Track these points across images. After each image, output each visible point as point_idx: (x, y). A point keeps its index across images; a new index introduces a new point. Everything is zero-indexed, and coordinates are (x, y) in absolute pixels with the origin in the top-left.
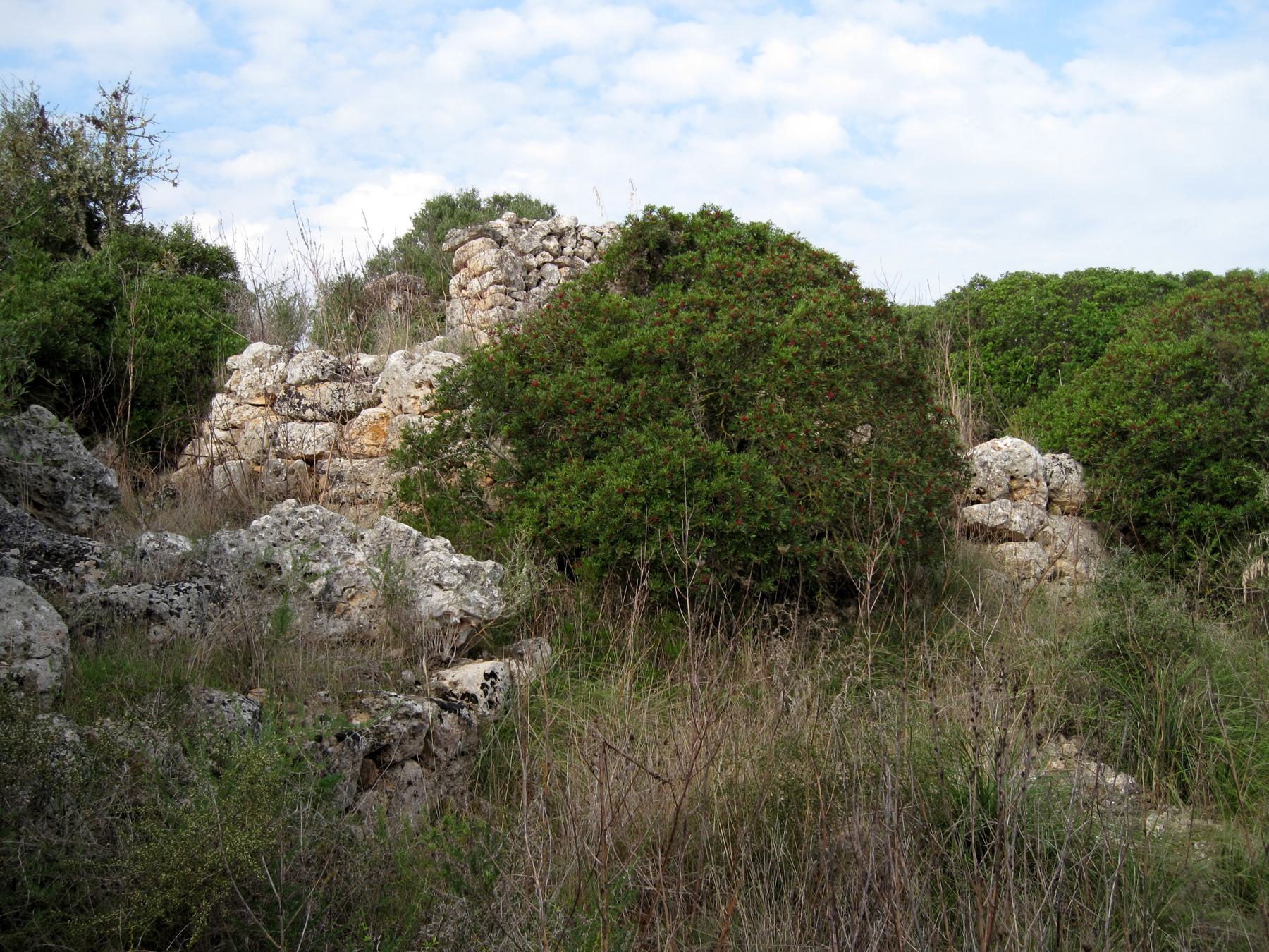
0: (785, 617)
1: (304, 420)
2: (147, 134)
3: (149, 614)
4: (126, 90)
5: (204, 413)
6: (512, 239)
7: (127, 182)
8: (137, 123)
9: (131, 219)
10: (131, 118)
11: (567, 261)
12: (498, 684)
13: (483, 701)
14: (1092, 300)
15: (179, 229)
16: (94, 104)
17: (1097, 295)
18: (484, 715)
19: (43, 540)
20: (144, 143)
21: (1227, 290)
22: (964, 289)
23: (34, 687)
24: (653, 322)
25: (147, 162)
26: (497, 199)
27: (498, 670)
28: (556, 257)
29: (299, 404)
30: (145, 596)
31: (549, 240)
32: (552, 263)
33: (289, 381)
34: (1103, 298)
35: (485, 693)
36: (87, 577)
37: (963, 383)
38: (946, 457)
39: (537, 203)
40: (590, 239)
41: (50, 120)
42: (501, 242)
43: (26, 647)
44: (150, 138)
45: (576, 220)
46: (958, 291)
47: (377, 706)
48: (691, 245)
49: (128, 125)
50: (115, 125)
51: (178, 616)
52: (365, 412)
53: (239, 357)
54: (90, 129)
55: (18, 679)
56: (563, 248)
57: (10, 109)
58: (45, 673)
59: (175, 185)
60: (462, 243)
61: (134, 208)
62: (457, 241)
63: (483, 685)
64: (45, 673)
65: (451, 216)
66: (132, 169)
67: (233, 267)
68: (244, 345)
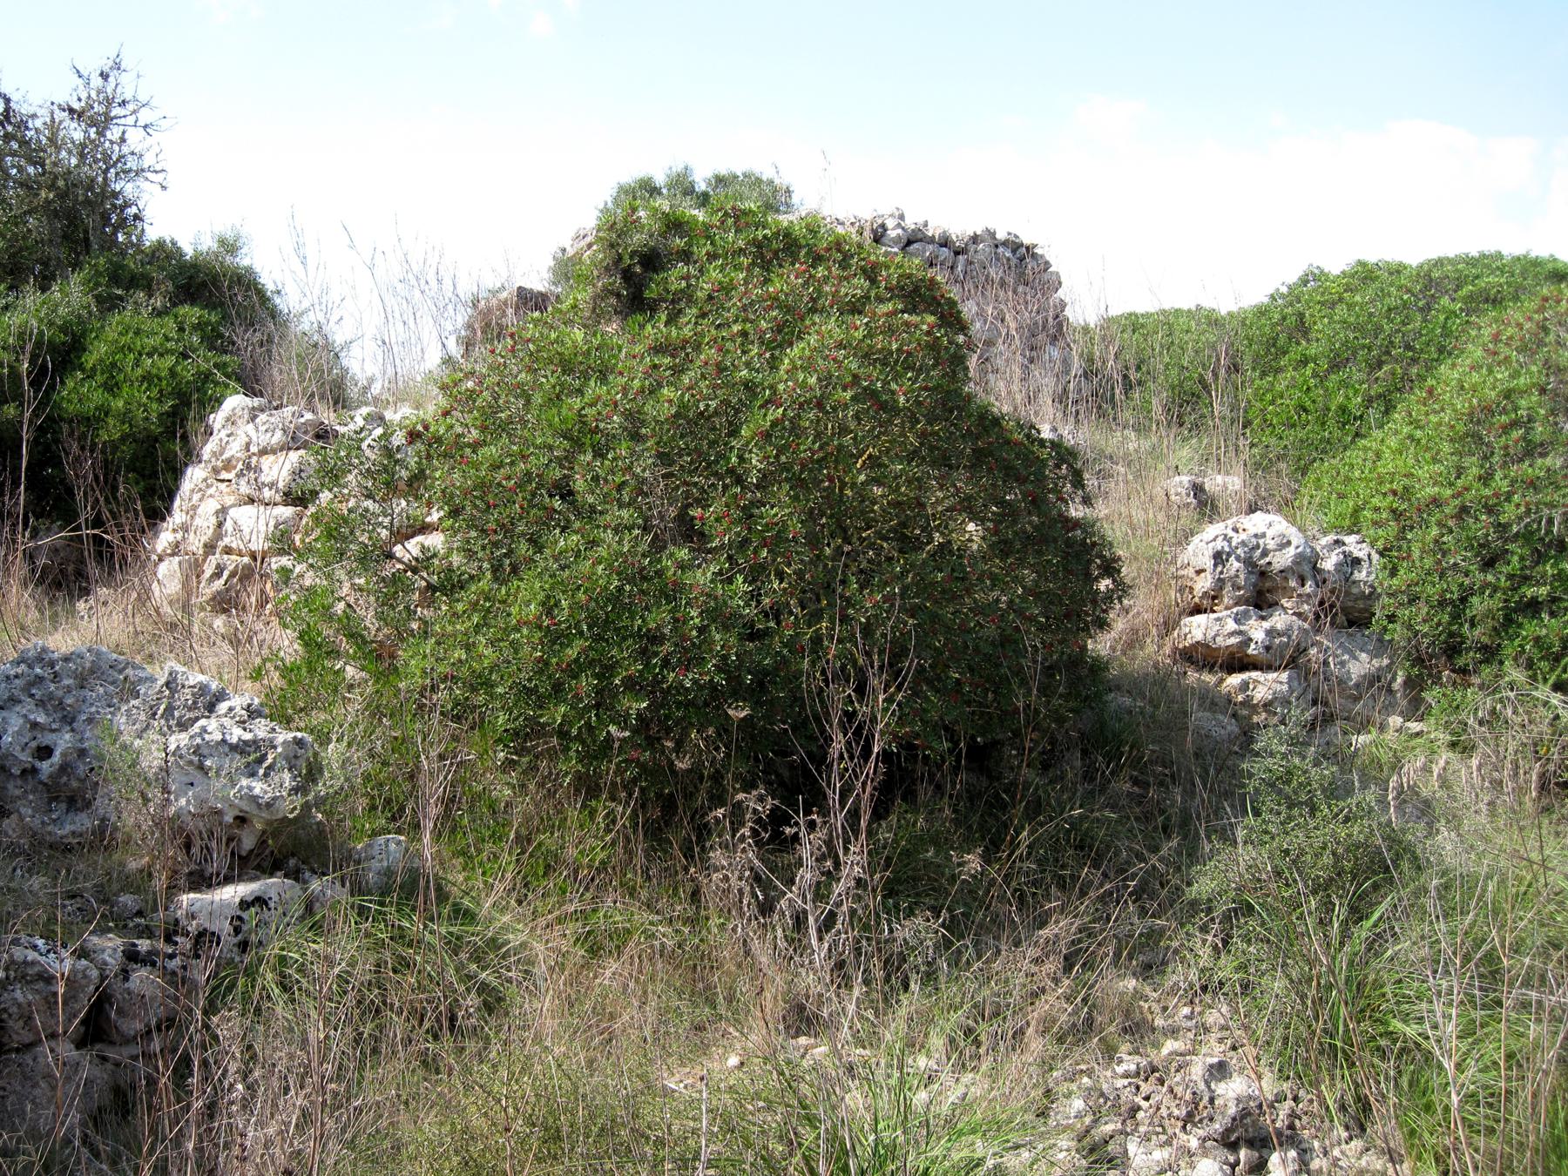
2: (141, 123)
4: (117, 66)
10: (123, 103)
14: (1453, 300)
15: (222, 242)
16: (67, 91)
26: (720, 180)
34: (1470, 298)
44: (145, 127)
46: (1284, 290)
59: (164, 188)
68: (219, 402)
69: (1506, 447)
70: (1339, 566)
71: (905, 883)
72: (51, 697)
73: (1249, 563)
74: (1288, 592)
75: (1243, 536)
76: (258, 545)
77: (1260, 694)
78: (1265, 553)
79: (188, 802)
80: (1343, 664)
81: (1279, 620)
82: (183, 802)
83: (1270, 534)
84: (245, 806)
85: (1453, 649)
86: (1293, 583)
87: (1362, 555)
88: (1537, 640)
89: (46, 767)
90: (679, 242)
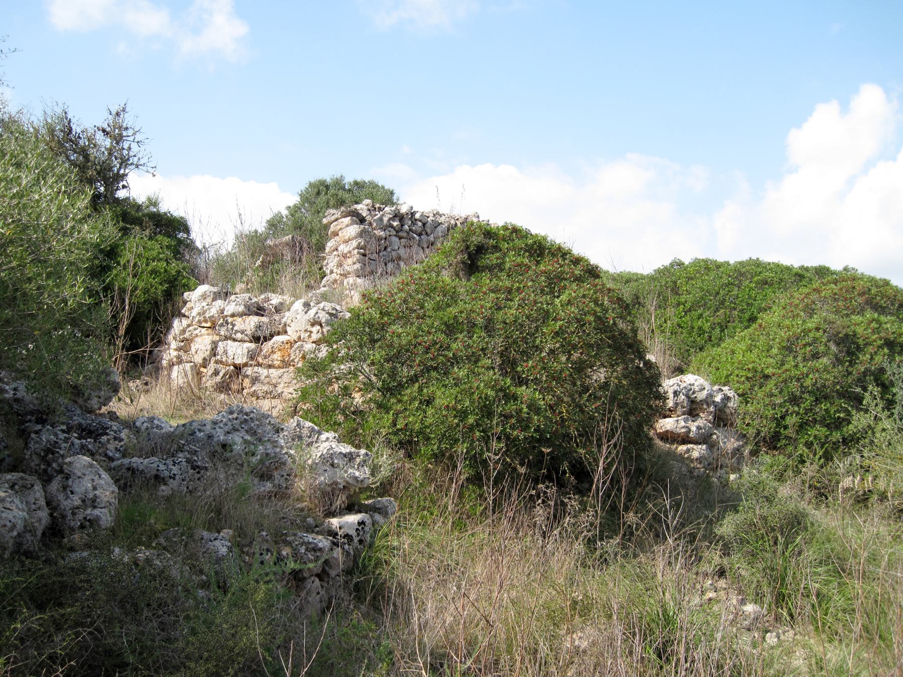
0: (545, 493)
1: (235, 340)
3: (157, 477)
5: (169, 328)
6: (368, 218)
7: (122, 172)
8: (130, 132)
9: (121, 194)
10: (127, 129)
11: (405, 235)
12: (367, 529)
13: (356, 540)
15: (149, 199)
16: (102, 119)
17: (755, 279)
18: (357, 548)
19: (81, 420)
20: (134, 146)
21: (839, 286)
22: (666, 268)
23: (99, 526)
24: (475, 297)
25: (136, 159)
26: (356, 183)
27: (366, 520)
28: (397, 232)
29: (232, 329)
30: (155, 465)
31: (394, 221)
32: (396, 236)
33: (225, 313)
35: (358, 535)
36: (109, 446)
37: (663, 332)
38: (647, 381)
39: (383, 187)
40: (420, 221)
41: (74, 127)
42: (362, 220)
43: (94, 500)
45: (412, 208)
47: (297, 543)
48: (496, 248)
49: (125, 133)
50: (116, 133)
51: (174, 479)
52: (276, 338)
53: (191, 293)
54: (100, 136)
55: (89, 520)
56: (402, 226)
57: (49, 121)
58: (105, 517)
60: (337, 220)
61: (124, 187)
62: (333, 218)
63: (357, 529)
64: (105, 517)
65: (326, 194)
66: (124, 162)
67: (187, 230)
69: (805, 353)
70: (722, 399)
71: (611, 524)
72: (251, 429)
73: (687, 396)
74: (703, 411)
75: (685, 385)
76: (239, 361)
77: (695, 455)
78: (694, 393)
79: (325, 479)
80: (725, 443)
81: (700, 422)
82: (323, 478)
83: (696, 384)
84: (351, 481)
85: (776, 436)
86: (705, 407)
87: (731, 395)
88: (815, 436)
89: (254, 460)
90: (492, 242)
